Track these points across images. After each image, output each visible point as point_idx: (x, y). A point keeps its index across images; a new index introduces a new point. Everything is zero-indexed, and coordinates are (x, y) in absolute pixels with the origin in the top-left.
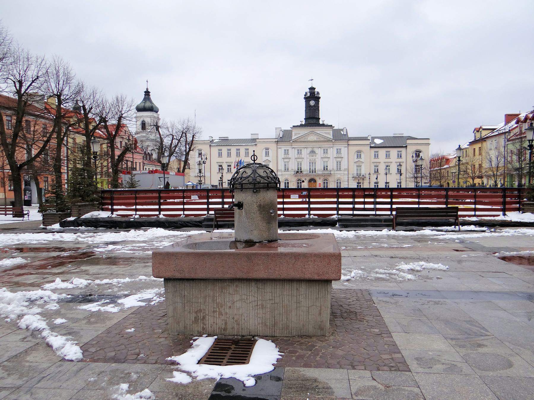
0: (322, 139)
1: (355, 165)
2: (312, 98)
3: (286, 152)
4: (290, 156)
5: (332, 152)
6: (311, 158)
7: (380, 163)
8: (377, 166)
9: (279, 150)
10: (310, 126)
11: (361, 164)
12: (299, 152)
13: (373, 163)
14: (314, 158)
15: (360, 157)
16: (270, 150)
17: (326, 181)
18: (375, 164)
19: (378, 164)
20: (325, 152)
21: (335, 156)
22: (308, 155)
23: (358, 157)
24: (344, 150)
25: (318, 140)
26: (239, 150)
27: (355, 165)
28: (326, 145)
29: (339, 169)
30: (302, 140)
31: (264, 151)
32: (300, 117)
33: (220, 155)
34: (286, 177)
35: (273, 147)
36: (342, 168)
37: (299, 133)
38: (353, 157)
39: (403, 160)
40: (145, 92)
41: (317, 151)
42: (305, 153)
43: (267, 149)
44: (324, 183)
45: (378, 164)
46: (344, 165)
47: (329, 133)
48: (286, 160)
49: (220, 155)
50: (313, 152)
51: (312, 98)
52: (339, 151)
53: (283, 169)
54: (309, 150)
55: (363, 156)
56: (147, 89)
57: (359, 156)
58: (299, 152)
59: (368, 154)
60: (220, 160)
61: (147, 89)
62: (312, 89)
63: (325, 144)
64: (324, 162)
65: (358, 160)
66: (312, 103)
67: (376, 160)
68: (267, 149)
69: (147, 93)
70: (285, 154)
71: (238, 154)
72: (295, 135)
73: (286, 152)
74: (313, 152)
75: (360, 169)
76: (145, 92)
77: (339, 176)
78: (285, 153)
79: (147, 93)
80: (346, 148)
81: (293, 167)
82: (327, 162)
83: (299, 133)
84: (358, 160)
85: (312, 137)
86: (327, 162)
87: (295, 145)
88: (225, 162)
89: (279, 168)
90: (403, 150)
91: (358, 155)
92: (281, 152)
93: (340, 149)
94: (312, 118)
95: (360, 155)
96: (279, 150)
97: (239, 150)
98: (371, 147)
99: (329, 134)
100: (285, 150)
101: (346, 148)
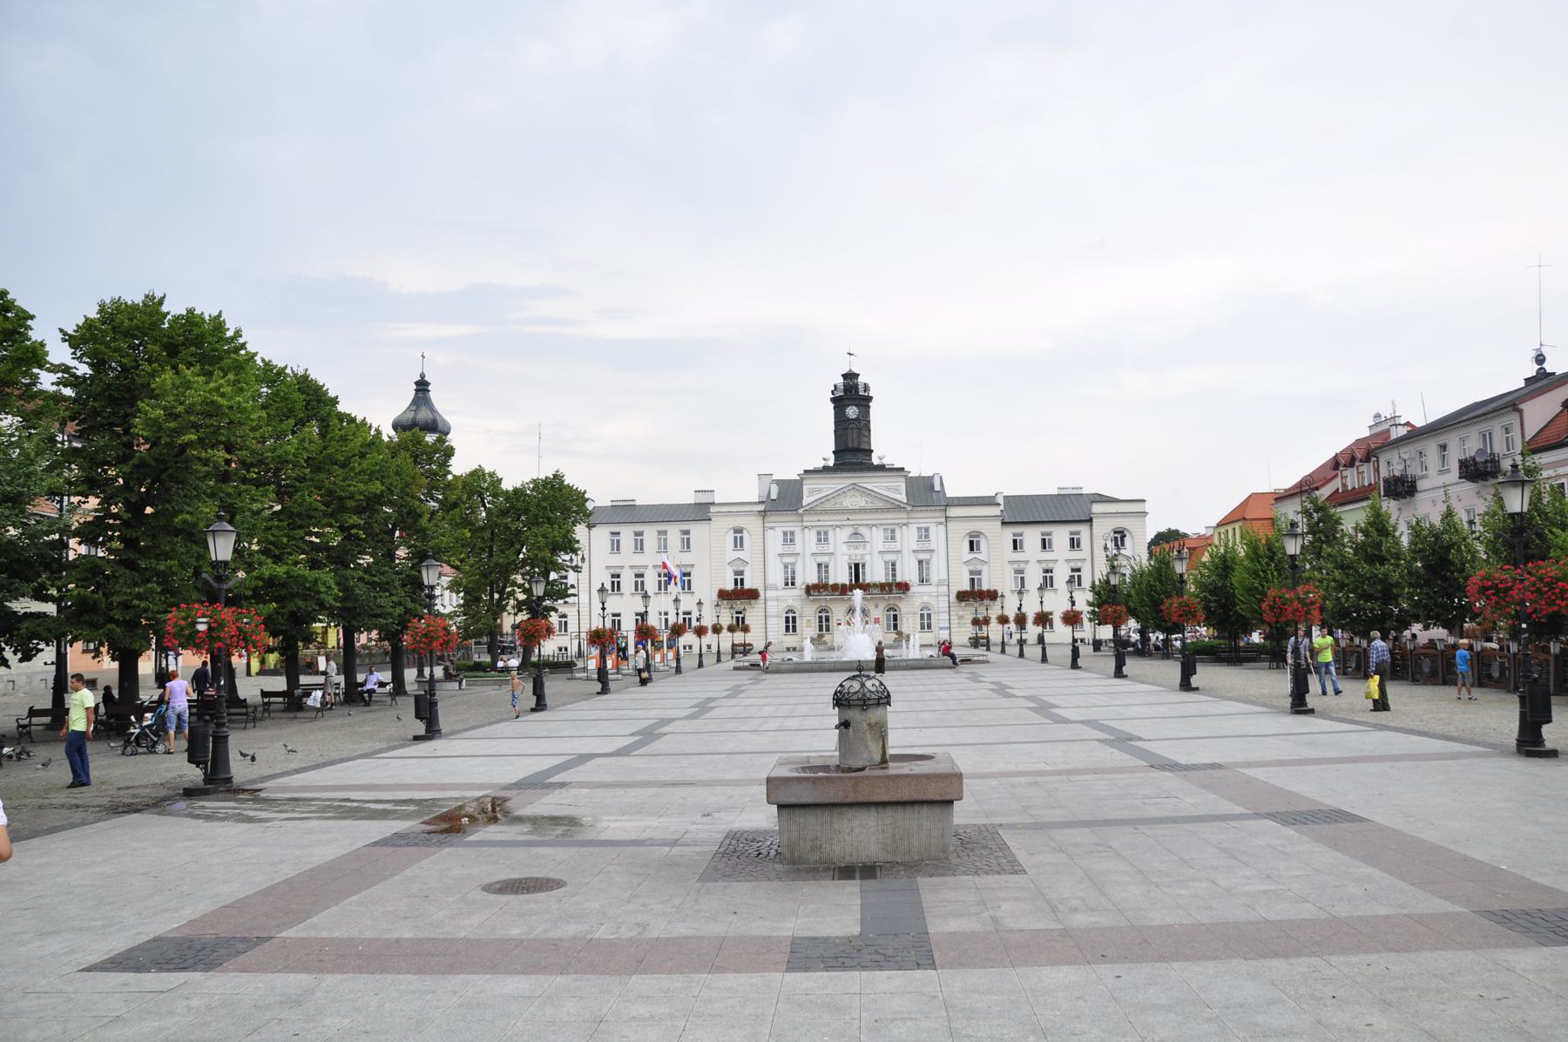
0: (880, 505)
2: (851, 399)
3: (789, 538)
4: (798, 548)
6: (853, 552)
8: (1022, 572)
10: (848, 471)
11: (979, 567)
14: (860, 551)
22: (845, 547)
24: (937, 533)
25: (870, 506)
28: (891, 518)
30: (828, 506)
31: (731, 535)
32: (823, 449)
33: (616, 547)
34: (790, 602)
35: (752, 525)
36: (934, 578)
37: (820, 490)
40: (417, 383)
43: (738, 531)
46: (937, 571)
47: (896, 490)
49: (616, 547)
51: (851, 399)
52: (924, 534)
56: (423, 376)
58: (822, 538)
59: (998, 539)
60: (615, 560)
61: (423, 376)
62: (850, 377)
63: (888, 516)
65: (972, 556)
66: (852, 412)
69: (422, 386)
76: (417, 383)
77: (926, 599)
79: (422, 386)
83: (820, 490)
87: (809, 520)
88: (627, 565)
89: (770, 581)
90: (1084, 530)
92: (775, 538)
96: (770, 533)
98: (1003, 523)
100: (785, 534)
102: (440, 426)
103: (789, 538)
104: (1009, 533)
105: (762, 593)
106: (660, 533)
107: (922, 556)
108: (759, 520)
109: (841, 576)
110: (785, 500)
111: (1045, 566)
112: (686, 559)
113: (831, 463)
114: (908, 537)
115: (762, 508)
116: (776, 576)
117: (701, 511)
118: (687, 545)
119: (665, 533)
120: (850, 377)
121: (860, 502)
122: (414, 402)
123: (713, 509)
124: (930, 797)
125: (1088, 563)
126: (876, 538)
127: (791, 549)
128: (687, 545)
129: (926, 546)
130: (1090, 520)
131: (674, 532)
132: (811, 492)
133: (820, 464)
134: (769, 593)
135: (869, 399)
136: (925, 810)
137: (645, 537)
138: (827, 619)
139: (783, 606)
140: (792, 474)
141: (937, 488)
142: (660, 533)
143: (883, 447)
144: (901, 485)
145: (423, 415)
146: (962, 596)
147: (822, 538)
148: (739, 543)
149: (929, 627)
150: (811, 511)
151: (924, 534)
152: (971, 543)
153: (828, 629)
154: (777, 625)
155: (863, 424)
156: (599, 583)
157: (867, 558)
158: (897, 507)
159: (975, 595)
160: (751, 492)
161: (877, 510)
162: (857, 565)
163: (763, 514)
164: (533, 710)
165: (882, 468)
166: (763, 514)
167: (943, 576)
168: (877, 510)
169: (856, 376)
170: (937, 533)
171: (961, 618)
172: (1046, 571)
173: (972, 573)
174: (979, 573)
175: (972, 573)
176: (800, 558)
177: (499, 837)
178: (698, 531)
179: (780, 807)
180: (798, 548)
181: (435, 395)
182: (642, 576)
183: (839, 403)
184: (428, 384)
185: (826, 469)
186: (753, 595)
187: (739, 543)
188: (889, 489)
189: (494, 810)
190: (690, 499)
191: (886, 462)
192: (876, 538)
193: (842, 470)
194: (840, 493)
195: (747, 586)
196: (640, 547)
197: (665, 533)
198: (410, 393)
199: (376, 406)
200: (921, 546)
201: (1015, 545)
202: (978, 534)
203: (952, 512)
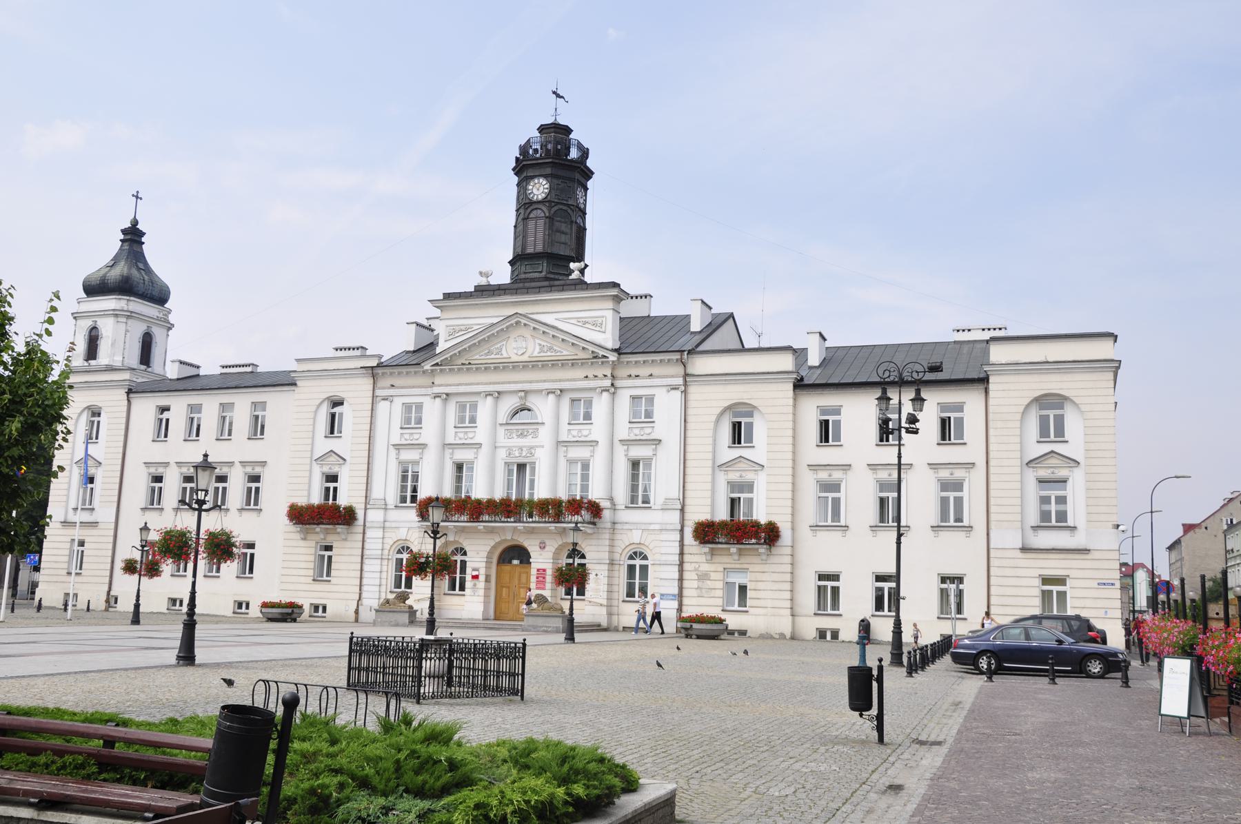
0: (566, 353)
1: (1031, 476)
3: (412, 417)
5: (609, 416)
6: (517, 441)
7: (847, 467)
8: (834, 487)
9: (383, 407)
11: (749, 476)
12: (467, 418)
13: (814, 467)
14: (527, 441)
15: (1060, 431)
16: (103, 419)
17: (638, 562)
18: (823, 475)
19: (837, 475)
21: (396, 440)
22: (501, 431)
23: (1044, 432)
24: (667, 405)
25: (549, 355)
27: (1031, 476)
28: (573, 378)
29: (638, 497)
33: (163, 429)
35: (357, 391)
36: (657, 498)
38: (709, 438)
39: (971, 449)
40: (124, 232)
41: (544, 408)
45: (837, 475)
46: (663, 483)
47: (597, 325)
48: (407, 455)
49: (163, 429)
51: (556, 168)
52: (643, 410)
53: (392, 496)
54: (510, 403)
55: (1073, 424)
56: (135, 223)
57: (1051, 429)
59: (780, 417)
60: (158, 452)
61: (135, 223)
62: (557, 133)
65: (736, 452)
67: (828, 455)
69: (133, 236)
70: (406, 424)
71: (194, 430)
72: (451, 334)
73: (412, 417)
75: (1062, 500)
76: (124, 232)
77: (636, 537)
79: (133, 236)
80: (677, 395)
82: (416, 463)
83: (467, 329)
84: (1046, 448)
86: (416, 463)
87: (446, 382)
89: (377, 493)
90: (971, 400)
91: (1044, 422)
92: (390, 414)
94: (550, 251)
95: (1060, 421)
98: (800, 385)
99: (595, 324)
100: (407, 407)
101: (677, 395)
104: (812, 407)
105: (360, 514)
107: (638, 452)
108: (365, 384)
109: (485, 485)
116: (387, 486)
118: (258, 428)
125: (978, 476)
129: (646, 432)
130: (984, 381)
135: (142, 234)
142: (255, 404)
146: (707, 533)
148: (333, 426)
152: (737, 427)
156: (100, 526)
159: (736, 533)
161: (555, 364)
162: (521, 467)
167: (675, 492)
168: (555, 364)
169: (567, 130)
170: (667, 405)
171: (703, 577)
173: (733, 486)
174: (749, 487)
175: (733, 486)
181: (150, 249)
183: (525, 167)
184: (142, 234)
185: (485, 291)
186: (347, 517)
187: (333, 426)
188: (584, 323)
189: (743, 633)
193: (527, 291)
195: (343, 501)
196: (225, 430)
198: (113, 244)
200: (636, 433)
201: (826, 432)
202: (750, 410)
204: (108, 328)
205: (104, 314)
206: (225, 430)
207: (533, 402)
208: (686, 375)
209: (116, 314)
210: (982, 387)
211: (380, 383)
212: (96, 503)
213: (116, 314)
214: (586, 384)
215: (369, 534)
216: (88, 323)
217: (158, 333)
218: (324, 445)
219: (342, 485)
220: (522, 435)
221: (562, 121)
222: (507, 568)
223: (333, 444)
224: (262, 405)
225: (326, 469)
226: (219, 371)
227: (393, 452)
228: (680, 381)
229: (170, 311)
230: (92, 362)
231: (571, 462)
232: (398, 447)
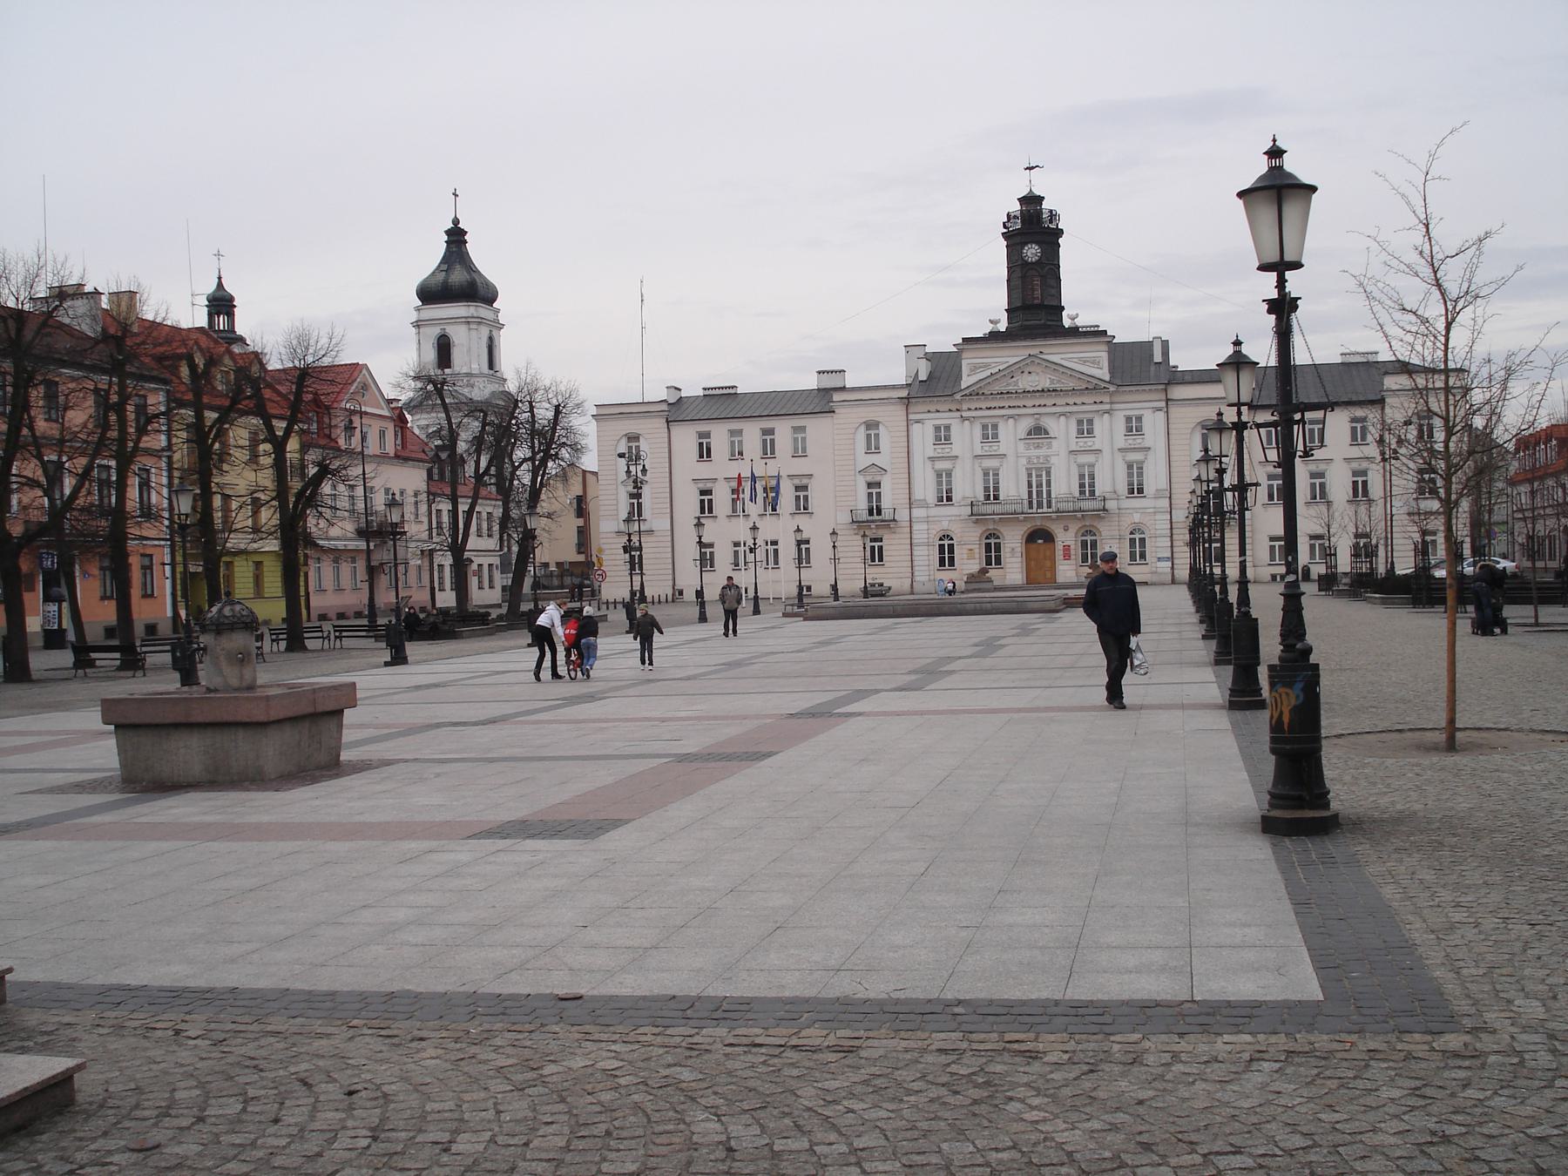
0: (1071, 384)
2: (1033, 234)
3: (943, 436)
4: (1096, 443)
6: (1034, 452)
8: (805, 488)
9: (916, 428)
14: (1042, 452)
16: (882, 430)
17: (946, 542)
20: (1085, 429)
22: (1021, 445)
24: (1153, 423)
26: (771, 432)
28: (1087, 404)
29: (1136, 490)
31: (861, 434)
32: (989, 304)
33: (705, 452)
34: (945, 525)
35: (891, 417)
36: (1149, 489)
37: (987, 366)
40: (448, 232)
42: (1011, 434)
43: (871, 425)
44: (1084, 544)
45: (805, 481)
47: (1095, 363)
48: (988, 463)
49: (705, 452)
50: (1038, 431)
51: (1033, 234)
52: (1134, 426)
53: (931, 497)
54: (1025, 424)
56: (456, 221)
58: (990, 434)
60: (704, 470)
61: (456, 221)
62: (1031, 202)
64: (1081, 466)
66: (1032, 252)
68: (871, 425)
69: (456, 236)
74: (1038, 431)
76: (448, 232)
77: (1137, 518)
78: (938, 438)
79: (456, 236)
80: (1161, 415)
81: (967, 486)
83: (987, 366)
85: (1033, 377)
86: (1092, 466)
89: (918, 494)
90: (1372, 414)
92: (923, 434)
93: (1139, 419)
96: (916, 428)
97: (771, 432)
100: (937, 428)
101: (1161, 415)
102: (482, 291)
103: (943, 436)
105: (902, 515)
106: (732, 433)
110: (937, 380)
111: (702, 486)
112: (800, 467)
113: (1003, 326)
114: (1109, 430)
115: (904, 393)
117: (824, 400)
118: (800, 452)
119: (740, 432)
120: (1031, 202)
121: (1042, 380)
122: (445, 260)
123: (837, 397)
124: (239, 718)
126: (1062, 430)
127: (944, 450)
128: (800, 452)
131: (783, 431)
132: (974, 369)
133: (981, 330)
134: (916, 513)
135: (1059, 233)
136: (241, 734)
137: (777, 437)
138: (998, 547)
139: (936, 531)
140: (944, 343)
141: (1158, 358)
142: (732, 433)
143: (1081, 297)
144: (1103, 356)
145: (458, 276)
147: (990, 434)
148: (872, 446)
149: (1143, 556)
150: (975, 393)
151: (1134, 426)
153: (998, 562)
154: (927, 557)
155: (1049, 269)
157: (1053, 460)
158: (1093, 387)
160: (896, 373)
163: (907, 401)
164: (387, 664)
165: (1074, 332)
166: (907, 401)
167: (1163, 484)
170: (1153, 423)
172: (703, 493)
176: (959, 461)
177: (61, 775)
178: (817, 428)
179: (119, 727)
180: (1096, 443)
182: (709, 492)
185: (994, 337)
187: (872, 446)
188: (1084, 362)
190: (810, 382)
191: (1079, 322)
192: (1062, 430)
194: (1011, 372)
196: (768, 450)
197: (740, 432)
198: (439, 248)
199: (178, 306)
203: (1179, 392)
204: (458, 335)
205: (454, 320)
206: (768, 450)
207: (1051, 424)
208: (1167, 400)
209: (467, 321)
210: (1378, 407)
211: (911, 409)
212: (646, 513)
213: (467, 321)
214: (1095, 407)
215: (915, 527)
216: (435, 331)
217: (494, 333)
218: (865, 460)
219: (886, 490)
220: (1038, 447)
221: (1037, 193)
222: (1033, 546)
223: (874, 459)
224: (802, 429)
225: (869, 479)
226: (701, 393)
227: (929, 464)
228: (1163, 404)
229: (498, 311)
230: (447, 371)
231: (1081, 466)
232: (932, 459)
